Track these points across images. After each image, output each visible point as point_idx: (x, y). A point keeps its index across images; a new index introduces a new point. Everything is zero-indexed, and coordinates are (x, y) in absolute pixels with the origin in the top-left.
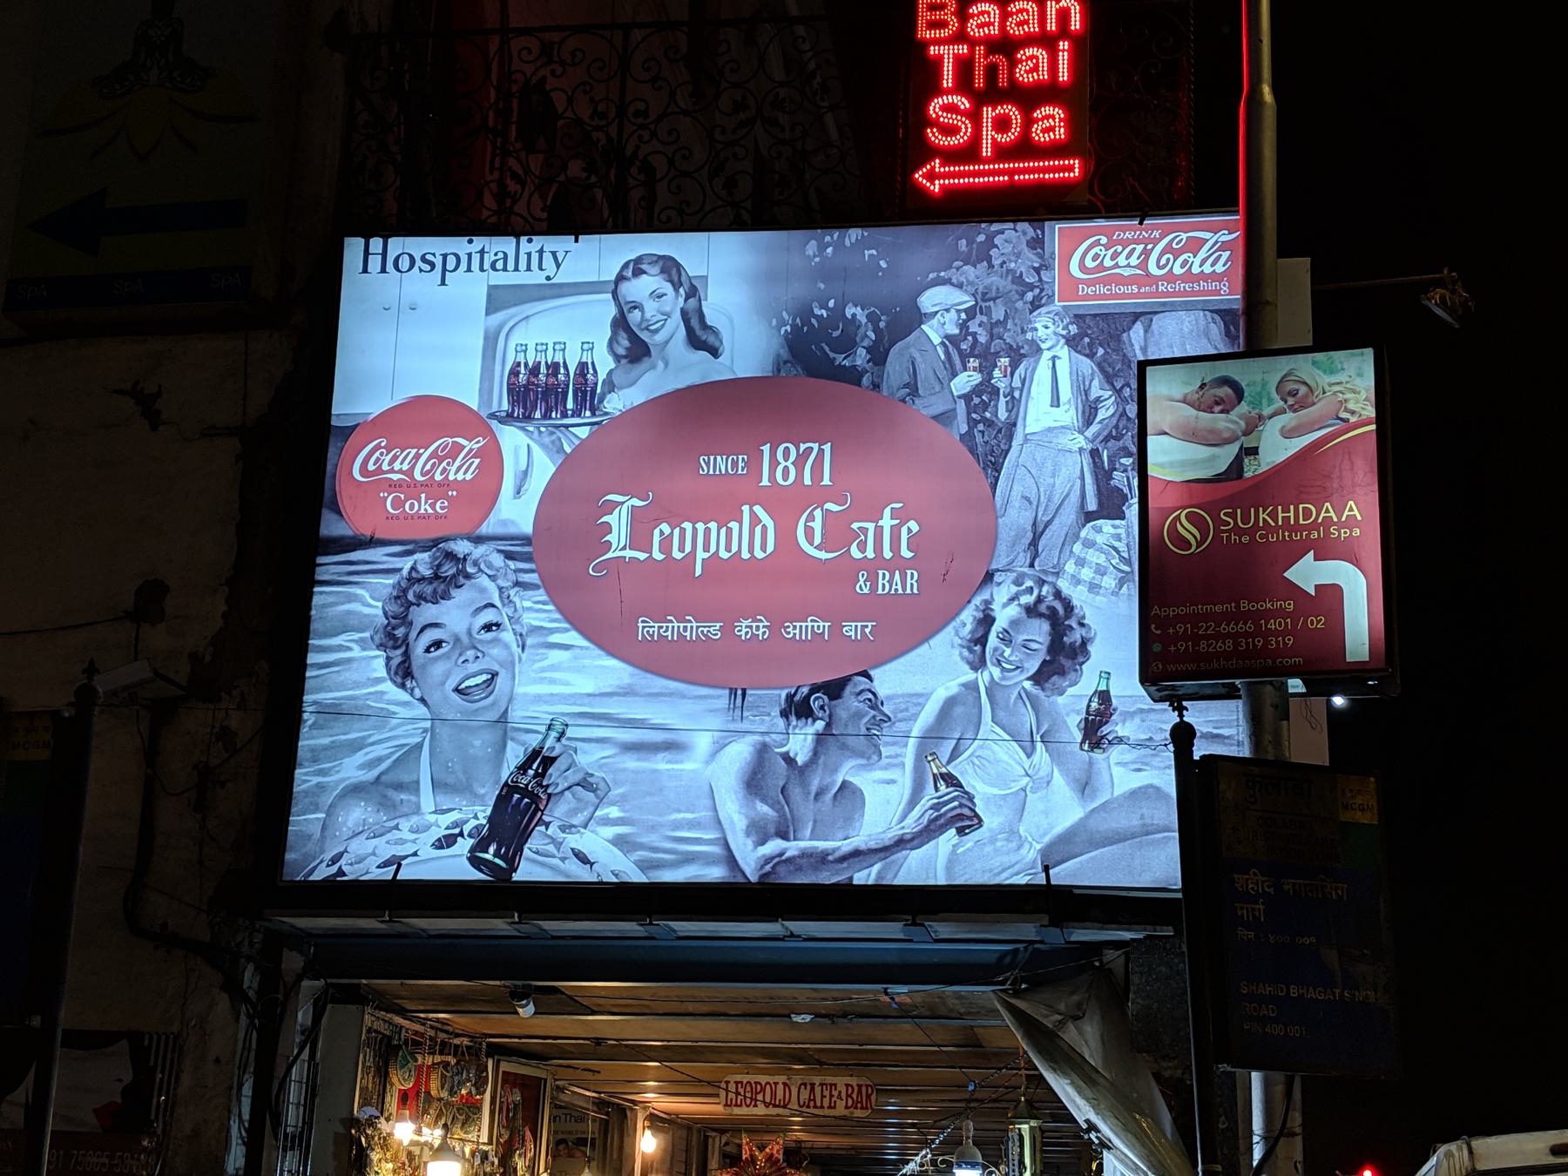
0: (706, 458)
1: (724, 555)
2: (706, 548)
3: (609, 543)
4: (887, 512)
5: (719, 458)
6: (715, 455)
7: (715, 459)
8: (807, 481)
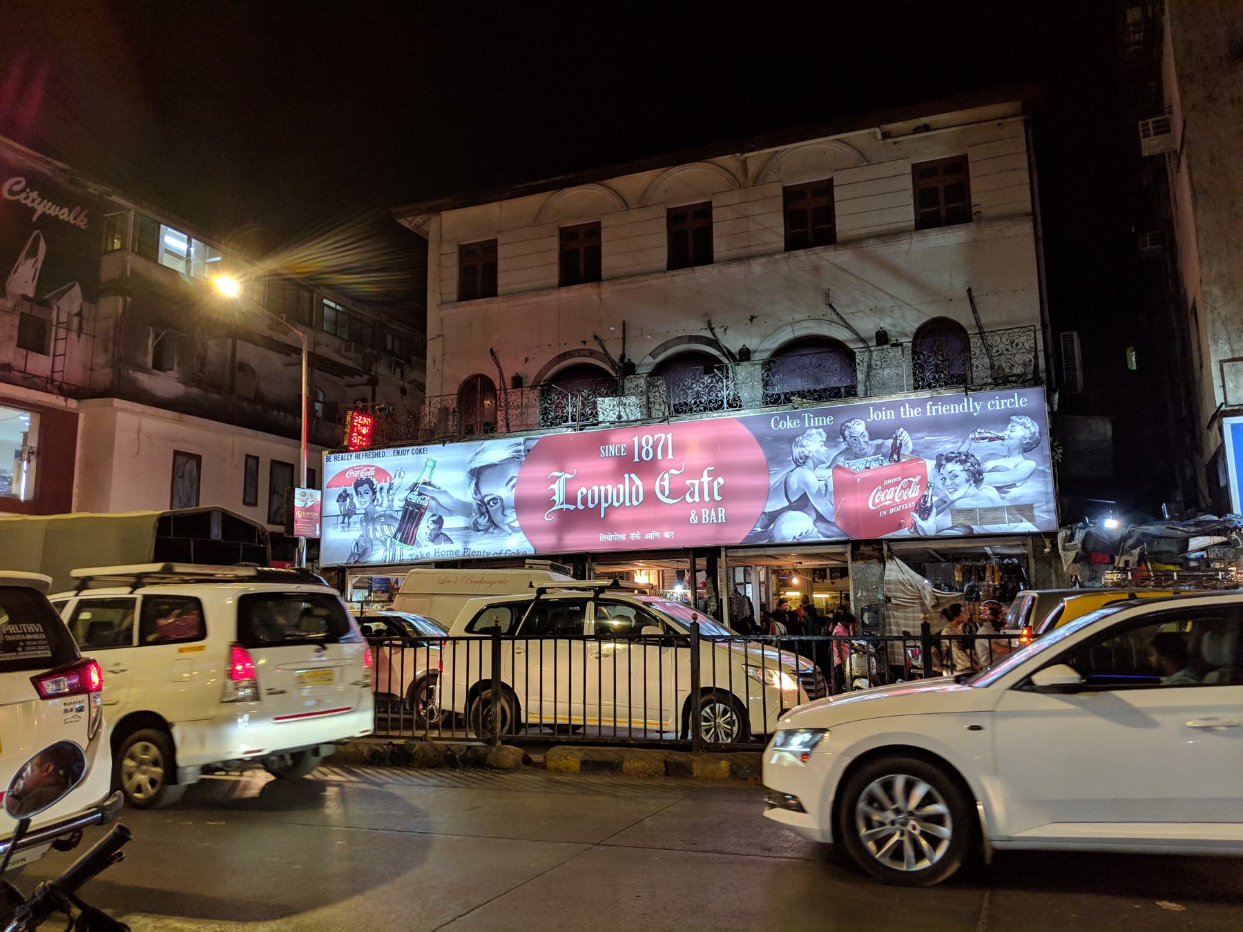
4: (705, 473)
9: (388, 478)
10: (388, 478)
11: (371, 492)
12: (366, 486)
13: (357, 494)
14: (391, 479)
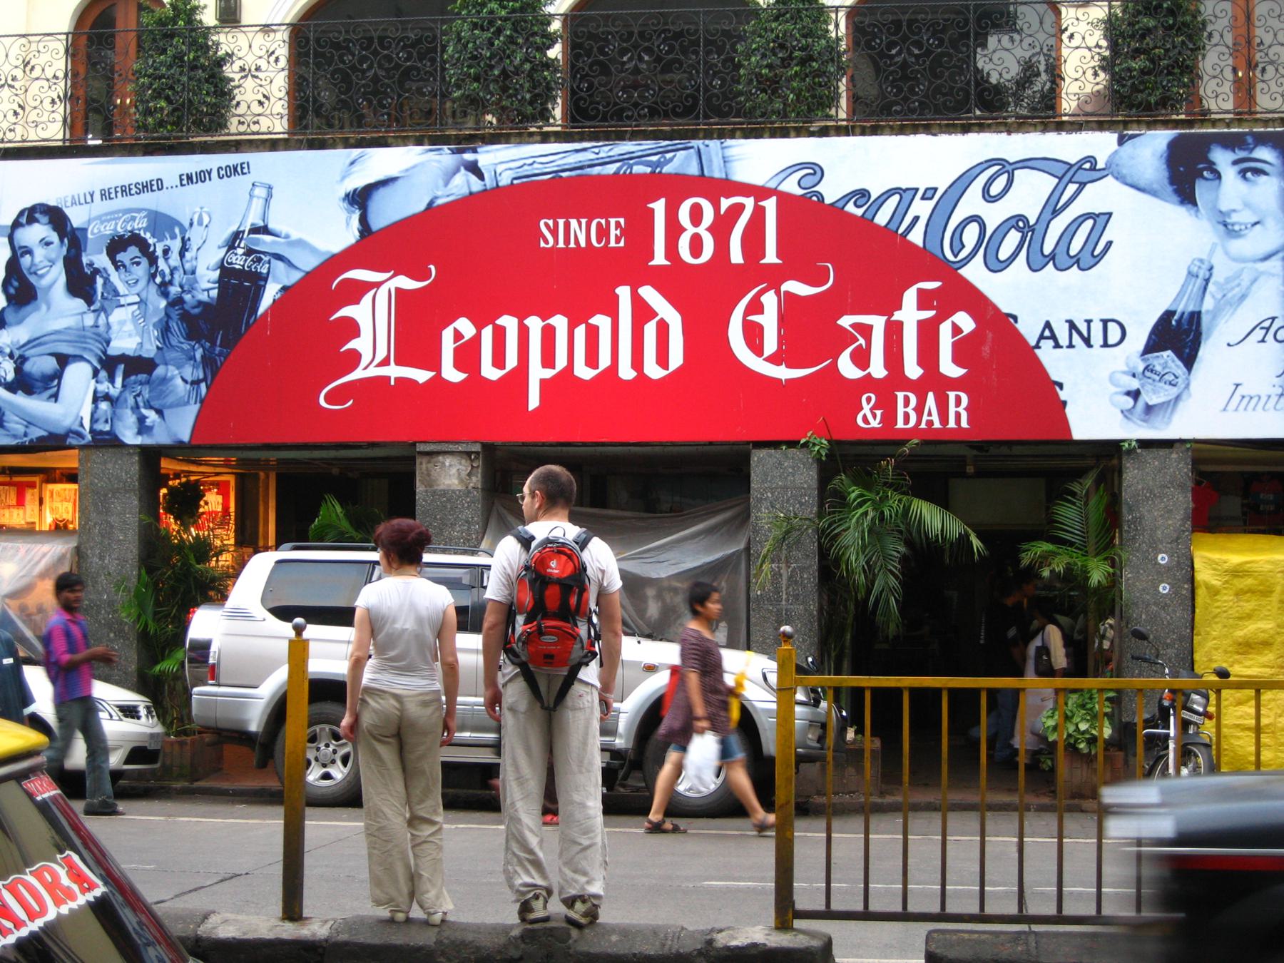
0: (551, 222)
1: (583, 372)
2: (548, 360)
3: (355, 357)
4: (910, 297)
5: (574, 222)
6: (568, 216)
7: (567, 226)
8: (736, 257)
9: (177, 230)
10: (177, 230)
11: (145, 262)
12: (133, 251)
13: (117, 268)
14: (183, 230)
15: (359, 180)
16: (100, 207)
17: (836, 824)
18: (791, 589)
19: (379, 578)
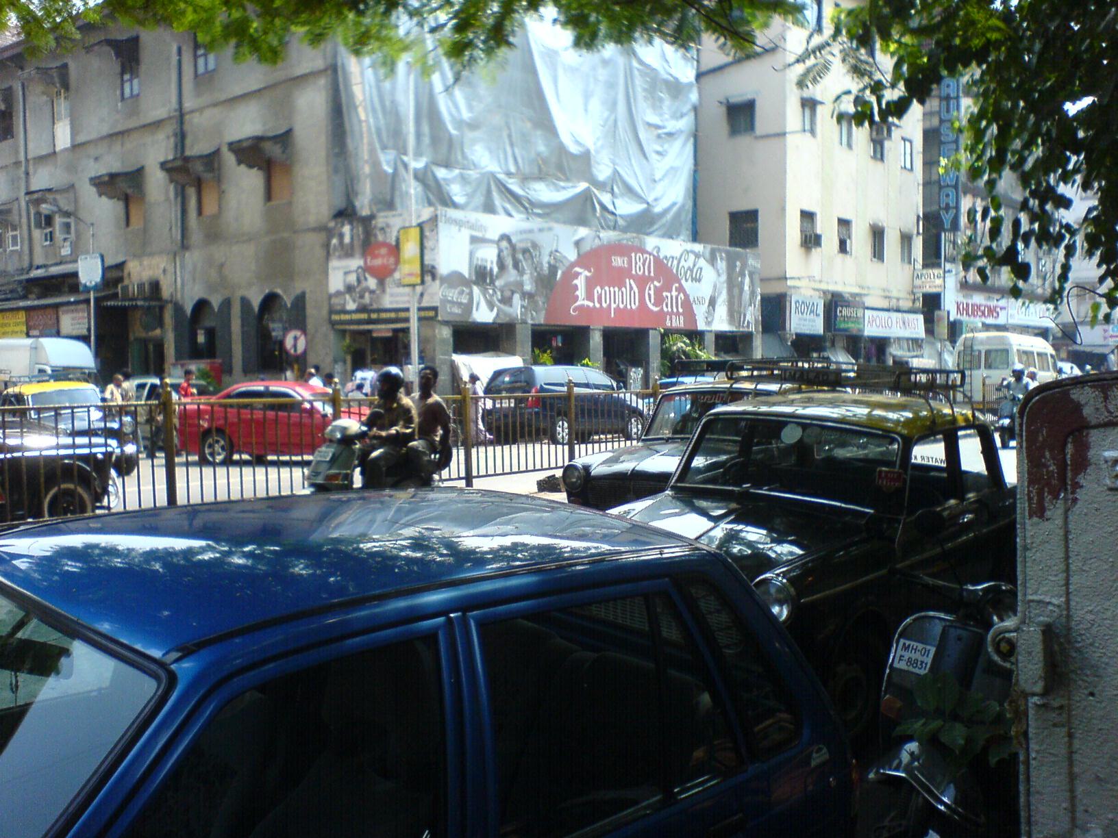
15: (577, 237)
16: (520, 237)
17: (293, 469)
18: (1088, 672)
19: (35, 172)
